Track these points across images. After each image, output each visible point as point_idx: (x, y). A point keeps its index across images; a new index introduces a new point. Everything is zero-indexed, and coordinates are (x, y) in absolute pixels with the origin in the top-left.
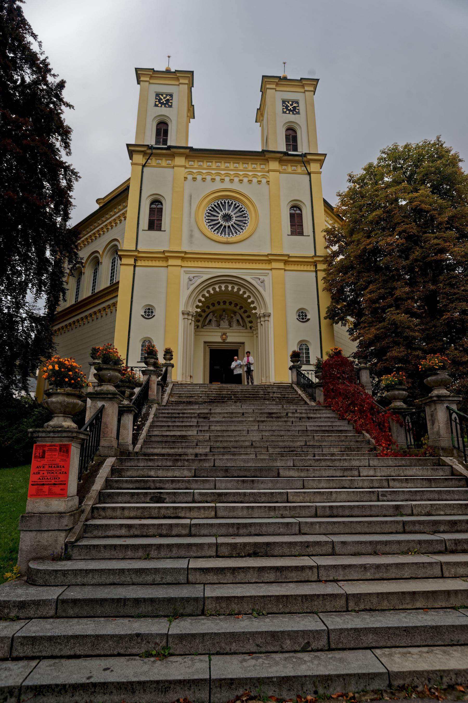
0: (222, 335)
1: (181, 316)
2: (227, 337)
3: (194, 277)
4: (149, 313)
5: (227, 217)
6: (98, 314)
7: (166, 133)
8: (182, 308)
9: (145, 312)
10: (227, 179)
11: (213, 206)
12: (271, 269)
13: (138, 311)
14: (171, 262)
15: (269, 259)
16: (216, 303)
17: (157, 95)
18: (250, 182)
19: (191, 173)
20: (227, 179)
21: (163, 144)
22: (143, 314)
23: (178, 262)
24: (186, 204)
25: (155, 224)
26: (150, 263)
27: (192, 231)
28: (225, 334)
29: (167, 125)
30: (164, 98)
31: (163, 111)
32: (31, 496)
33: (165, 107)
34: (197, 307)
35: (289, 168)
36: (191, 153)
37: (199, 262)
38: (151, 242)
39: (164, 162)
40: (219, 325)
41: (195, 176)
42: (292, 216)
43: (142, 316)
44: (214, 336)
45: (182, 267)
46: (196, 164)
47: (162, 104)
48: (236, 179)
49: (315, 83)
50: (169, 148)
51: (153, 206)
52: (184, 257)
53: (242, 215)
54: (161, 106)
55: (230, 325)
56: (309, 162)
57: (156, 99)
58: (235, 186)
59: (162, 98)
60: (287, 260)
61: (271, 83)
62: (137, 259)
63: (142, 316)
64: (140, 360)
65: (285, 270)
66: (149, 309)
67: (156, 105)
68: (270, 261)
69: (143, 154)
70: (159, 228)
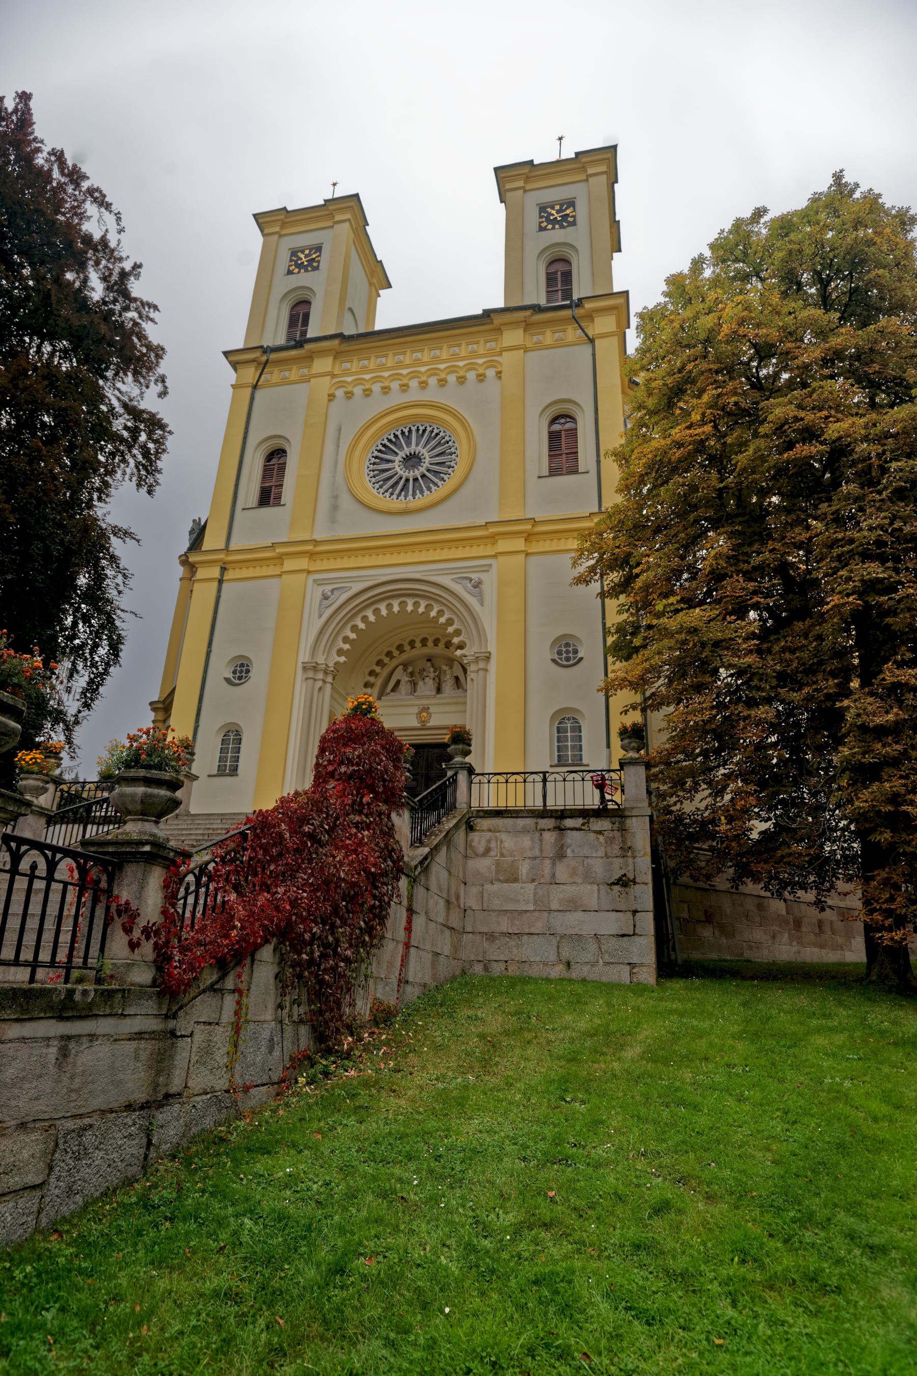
0: (420, 713)
2: (430, 714)
3: (332, 591)
4: (241, 671)
5: (412, 460)
7: (567, 277)
8: (304, 656)
9: (234, 672)
10: (414, 384)
11: (386, 442)
12: (495, 556)
13: (221, 669)
14: (289, 565)
16: (406, 644)
17: (542, 209)
18: (462, 380)
19: (342, 385)
20: (414, 384)
21: (563, 300)
22: (230, 676)
23: (303, 563)
24: (329, 447)
26: (251, 573)
27: (336, 497)
28: (425, 709)
29: (568, 262)
30: (558, 212)
31: (557, 235)
33: (562, 227)
35: (549, 337)
36: (345, 347)
37: (360, 558)
39: (294, 373)
41: (350, 389)
42: (554, 438)
43: (554, 661)
45: (309, 572)
46: (354, 365)
47: (555, 222)
48: (433, 381)
49: (609, 155)
50: (580, 303)
51: (556, 427)
52: (314, 551)
54: (553, 228)
56: (590, 317)
57: (541, 217)
58: (432, 394)
59: (554, 212)
61: (512, 178)
62: (227, 566)
63: (227, 680)
64: (215, 772)
65: (527, 554)
66: (242, 665)
67: (542, 229)
68: (493, 538)
69: (255, 364)
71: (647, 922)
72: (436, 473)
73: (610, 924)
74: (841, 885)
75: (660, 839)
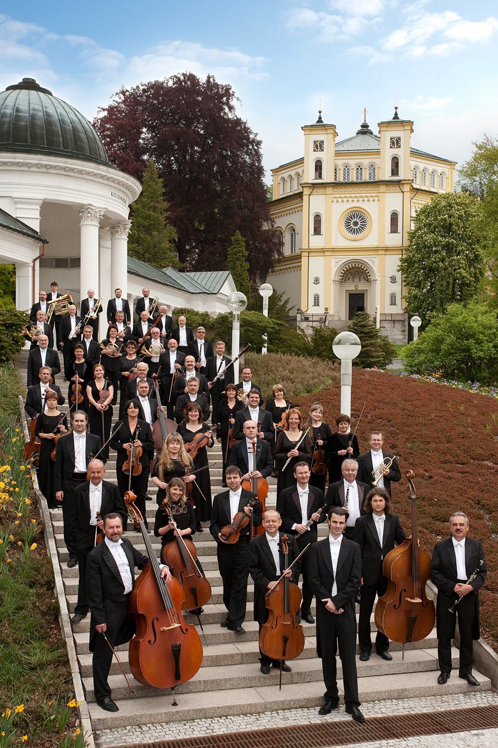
1: (332, 282)
4: (317, 281)
5: (356, 224)
6: (286, 271)
8: (333, 279)
13: (312, 280)
15: (377, 249)
25: (317, 231)
28: (357, 285)
32: (178, 342)
34: (340, 276)
38: (317, 242)
40: (353, 281)
44: (351, 287)
52: (333, 250)
53: (364, 222)
55: (360, 280)
60: (387, 249)
70: (318, 305)
71: (407, 337)
72: (362, 228)
73: (401, 337)
74: (309, 332)
75: (137, 433)
